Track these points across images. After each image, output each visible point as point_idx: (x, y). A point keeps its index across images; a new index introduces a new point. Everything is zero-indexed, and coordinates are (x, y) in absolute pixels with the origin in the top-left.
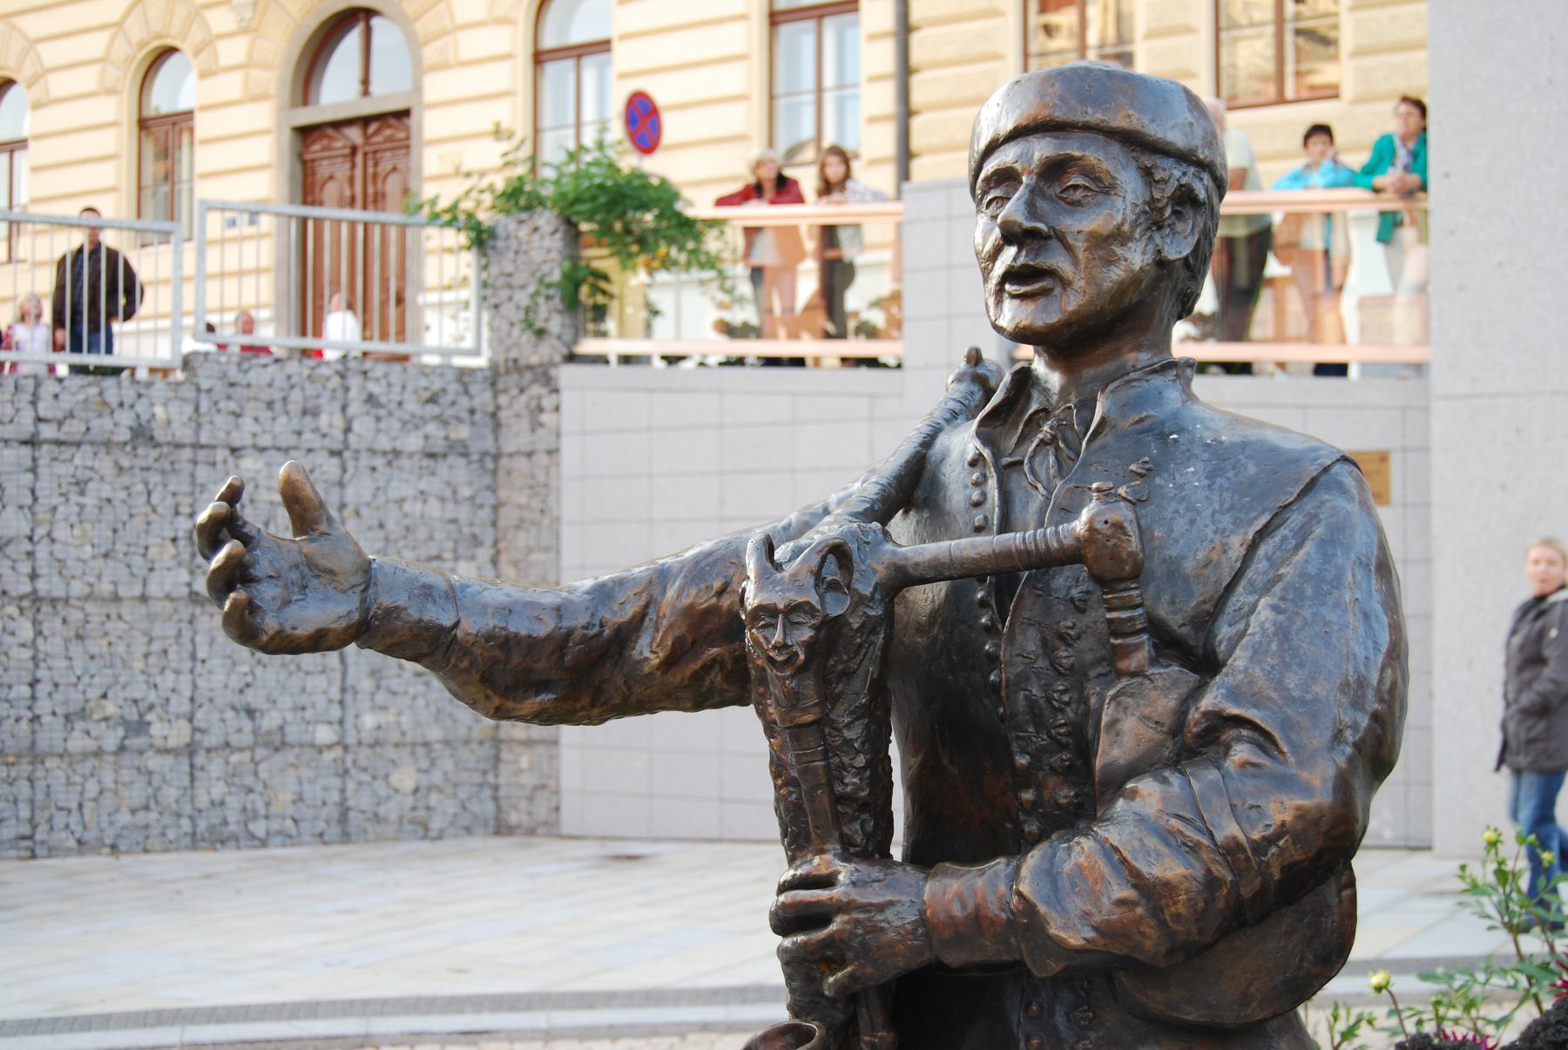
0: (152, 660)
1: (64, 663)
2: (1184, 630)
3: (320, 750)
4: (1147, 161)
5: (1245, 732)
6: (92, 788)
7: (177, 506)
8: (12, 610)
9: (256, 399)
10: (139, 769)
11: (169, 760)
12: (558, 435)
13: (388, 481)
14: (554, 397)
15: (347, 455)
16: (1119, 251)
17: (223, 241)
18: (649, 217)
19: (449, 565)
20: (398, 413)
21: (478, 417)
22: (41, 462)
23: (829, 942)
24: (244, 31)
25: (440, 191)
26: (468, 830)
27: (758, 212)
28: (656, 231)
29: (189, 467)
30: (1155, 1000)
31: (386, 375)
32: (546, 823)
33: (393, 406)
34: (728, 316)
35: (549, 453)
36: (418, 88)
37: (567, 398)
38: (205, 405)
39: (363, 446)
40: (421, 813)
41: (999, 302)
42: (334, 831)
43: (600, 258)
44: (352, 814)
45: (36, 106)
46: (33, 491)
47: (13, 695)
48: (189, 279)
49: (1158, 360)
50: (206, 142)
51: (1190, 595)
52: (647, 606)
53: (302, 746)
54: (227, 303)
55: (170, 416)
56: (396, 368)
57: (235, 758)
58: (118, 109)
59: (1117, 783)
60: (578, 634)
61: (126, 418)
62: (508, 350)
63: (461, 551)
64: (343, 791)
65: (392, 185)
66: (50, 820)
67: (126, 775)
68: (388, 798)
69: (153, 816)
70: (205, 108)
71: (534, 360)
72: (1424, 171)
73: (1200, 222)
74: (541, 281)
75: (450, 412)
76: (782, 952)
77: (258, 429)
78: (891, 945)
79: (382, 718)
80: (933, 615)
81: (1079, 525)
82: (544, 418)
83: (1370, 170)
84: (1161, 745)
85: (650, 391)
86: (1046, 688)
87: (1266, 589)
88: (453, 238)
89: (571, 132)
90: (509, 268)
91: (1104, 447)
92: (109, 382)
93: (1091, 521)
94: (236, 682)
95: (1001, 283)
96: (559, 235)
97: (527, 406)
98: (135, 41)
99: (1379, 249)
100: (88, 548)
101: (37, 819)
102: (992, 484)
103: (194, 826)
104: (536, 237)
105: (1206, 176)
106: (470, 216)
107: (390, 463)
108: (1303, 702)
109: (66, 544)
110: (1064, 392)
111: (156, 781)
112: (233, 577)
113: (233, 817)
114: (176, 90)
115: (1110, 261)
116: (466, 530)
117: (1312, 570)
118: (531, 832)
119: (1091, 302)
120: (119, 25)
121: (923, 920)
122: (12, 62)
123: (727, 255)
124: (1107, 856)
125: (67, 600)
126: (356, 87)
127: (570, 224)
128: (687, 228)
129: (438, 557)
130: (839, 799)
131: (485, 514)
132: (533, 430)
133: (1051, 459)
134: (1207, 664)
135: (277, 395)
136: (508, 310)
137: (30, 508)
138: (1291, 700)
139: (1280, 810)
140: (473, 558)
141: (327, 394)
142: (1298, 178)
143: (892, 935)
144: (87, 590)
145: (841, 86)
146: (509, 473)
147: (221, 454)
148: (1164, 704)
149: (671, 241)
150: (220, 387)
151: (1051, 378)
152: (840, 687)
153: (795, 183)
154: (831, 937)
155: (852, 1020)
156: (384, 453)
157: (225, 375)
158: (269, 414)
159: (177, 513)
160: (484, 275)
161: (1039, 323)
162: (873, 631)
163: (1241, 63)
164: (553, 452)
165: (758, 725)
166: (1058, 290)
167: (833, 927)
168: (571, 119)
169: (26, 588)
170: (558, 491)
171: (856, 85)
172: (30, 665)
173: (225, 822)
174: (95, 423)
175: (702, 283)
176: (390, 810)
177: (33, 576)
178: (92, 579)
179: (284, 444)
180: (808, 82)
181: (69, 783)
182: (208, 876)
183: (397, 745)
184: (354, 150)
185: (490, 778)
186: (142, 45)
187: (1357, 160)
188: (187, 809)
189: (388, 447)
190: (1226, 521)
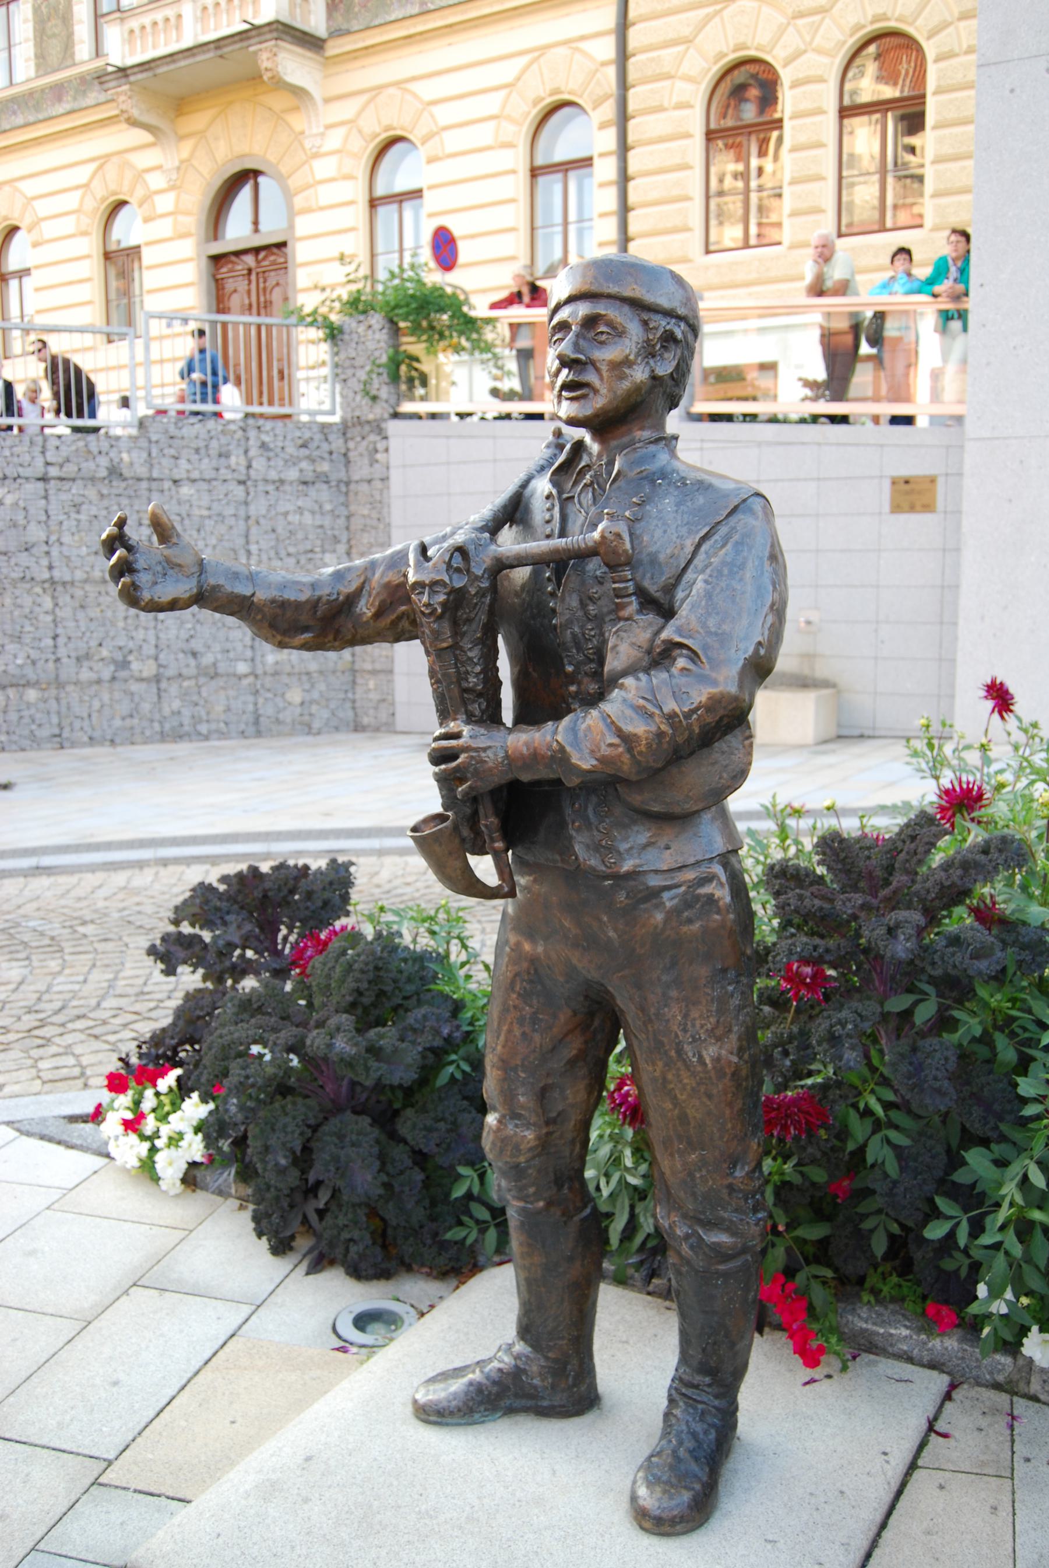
0: (130, 621)
1: (72, 624)
2: (658, 595)
3: (240, 678)
4: (645, 316)
5: (684, 651)
6: (96, 704)
7: (140, 519)
8: (38, 590)
9: (188, 447)
10: (125, 691)
11: (143, 686)
12: (388, 468)
13: (277, 500)
14: (384, 442)
15: (249, 483)
16: (627, 371)
17: (161, 338)
18: (445, 317)
19: (319, 556)
20: (282, 455)
21: (334, 456)
22: (51, 492)
23: (457, 769)
24: (172, 188)
25: (308, 301)
26: (337, 729)
27: (519, 313)
28: (449, 327)
29: (146, 493)
30: (636, 799)
31: (273, 429)
32: (386, 724)
33: (279, 450)
34: (498, 385)
35: (382, 480)
36: (291, 227)
37: (393, 443)
39: (259, 478)
40: (306, 718)
41: (559, 402)
42: (251, 730)
43: (413, 346)
44: (262, 719)
46: (46, 512)
47: (42, 645)
48: (141, 364)
49: (655, 435)
50: (149, 268)
51: (662, 574)
52: (364, 583)
53: (228, 675)
54: (166, 381)
55: (131, 459)
56: (279, 424)
57: (186, 684)
58: (90, 246)
59: (613, 682)
60: (325, 599)
61: (104, 461)
62: (353, 410)
63: (327, 547)
64: (256, 704)
65: (276, 296)
66: (71, 724)
67: (117, 695)
68: (285, 708)
69: (136, 721)
70: (148, 244)
71: (371, 417)
72: (967, 283)
73: (679, 352)
74: (374, 363)
75: (316, 453)
76: (435, 774)
77: (190, 467)
78: (490, 769)
80: (523, 586)
81: (596, 535)
82: (379, 456)
83: (931, 281)
84: (641, 659)
85: (448, 437)
86: (582, 627)
87: (703, 571)
88: (315, 334)
89: (396, 255)
90: (353, 354)
91: (619, 488)
92: (91, 437)
93: (603, 532)
94: (184, 635)
95: (561, 391)
96: (385, 331)
97: (367, 449)
98: (99, 196)
99: (937, 337)
100: (84, 549)
101: (63, 724)
102: (557, 509)
103: (162, 727)
104: (370, 332)
105: (682, 325)
106: (325, 318)
107: (277, 489)
108: (716, 634)
109: (70, 546)
110: (600, 456)
111: (137, 699)
112: (123, 569)
113: (186, 721)
114: (128, 231)
115: (622, 377)
116: (329, 532)
117: (728, 559)
118: (377, 729)
119: (610, 402)
120: (87, 186)
121: (507, 756)
122: (16, 215)
123: (498, 342)
124: (604, 719)
125: (72, 583)
126: (250, 227)
127: (392, 322)
128: (469, 325)
129: (311, 551)
130: (466, 690)
131: (342, 522)
132: (371, 465)
133: (590, 495)
134: (668, 613)
135: (202, 444)
136: (353, 383)
137: (46, 522)
138: (709, 633)
139: (700, 695)
140: (334, 551)
141: (235, 442)
142: (886, 286)
143: (491, 764)
144: (85, 576)
145: (580, 221)
146: (356, 494)
147: (167, 485)
148: (643, 636)
149: (461, 333)
150: (164, 439)
151: (595, 447)
152: (465, 628)
153: (545, 290)
154: (458, 766)
155: (476, 813)
156: (274, 482)
157: (166, 431)
158: (197, 457)
159: (140, 524)
160: (336, 359)
161: (581, 415)
162: (484, 596)
163: (857, 201)
164: (385, 479)
165: (422, 648)
166: (591, 395)
167: (459, 760)
168: (396, 247)
169: (46, 575)
170: (389, 506)
171: (591, 220)
172: (52, 625)
173: (182, 725)
174: (84, 465)
175: (483, 362)
176: (287, 716)
177: (50, 568)
178: (88, 569)
179: (207, 477)
180: (558, 218)
181: (81, 701)
182: (172, 759)
183: (289, 674)
184: (250, 271)
185: (350, 695)
186: (103, 199)
187: (923, 272)
188: (157, 717)
189: (276, 478)
190: (684, 531)
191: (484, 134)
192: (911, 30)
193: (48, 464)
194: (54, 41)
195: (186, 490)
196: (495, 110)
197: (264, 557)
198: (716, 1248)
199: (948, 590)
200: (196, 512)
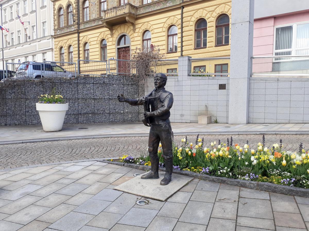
1: (97, 105)
6: (100, 117)
38: (110, 80)
45: (90, 45)
61: (102, 81)
79: (128, 110)
94: (113, 107)
120: (98, 36)
141: (122, 79)
147: (112, 84)
191: (160, 30)
192: (227, 14)
193: (94, 81)
194: (94, 14)
195: (114, 85)
196: (162, 26)
197: (126, 96)
198: (168, 158)
199: (228, 101)
200: (116, 89)
